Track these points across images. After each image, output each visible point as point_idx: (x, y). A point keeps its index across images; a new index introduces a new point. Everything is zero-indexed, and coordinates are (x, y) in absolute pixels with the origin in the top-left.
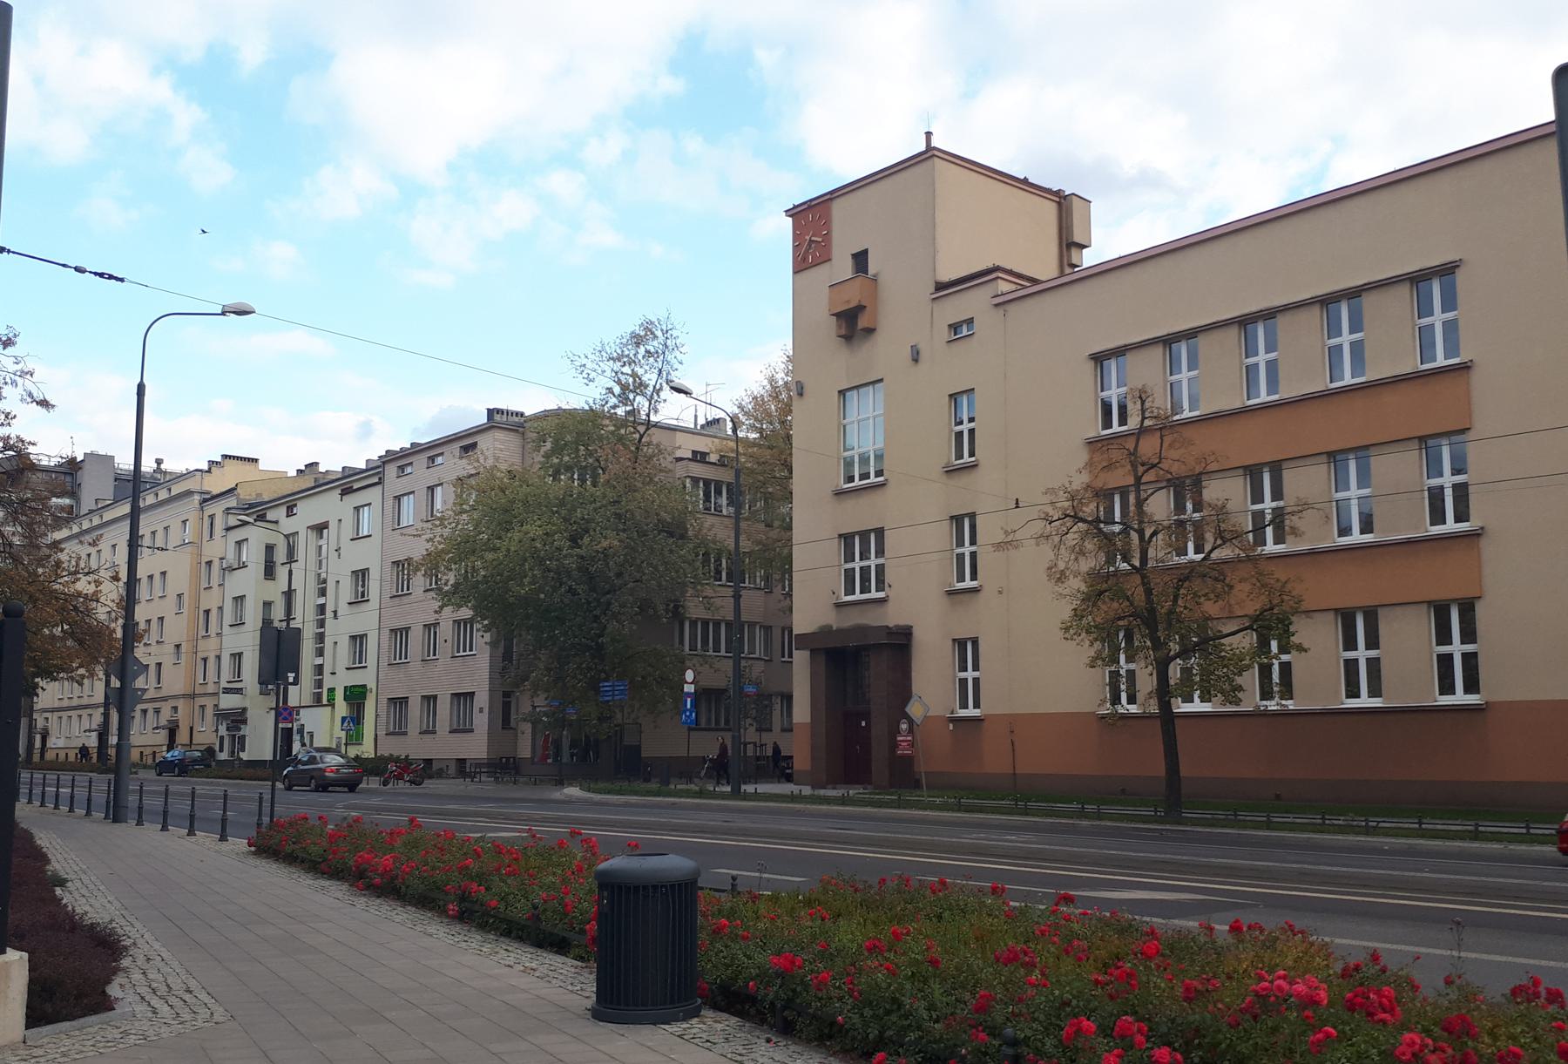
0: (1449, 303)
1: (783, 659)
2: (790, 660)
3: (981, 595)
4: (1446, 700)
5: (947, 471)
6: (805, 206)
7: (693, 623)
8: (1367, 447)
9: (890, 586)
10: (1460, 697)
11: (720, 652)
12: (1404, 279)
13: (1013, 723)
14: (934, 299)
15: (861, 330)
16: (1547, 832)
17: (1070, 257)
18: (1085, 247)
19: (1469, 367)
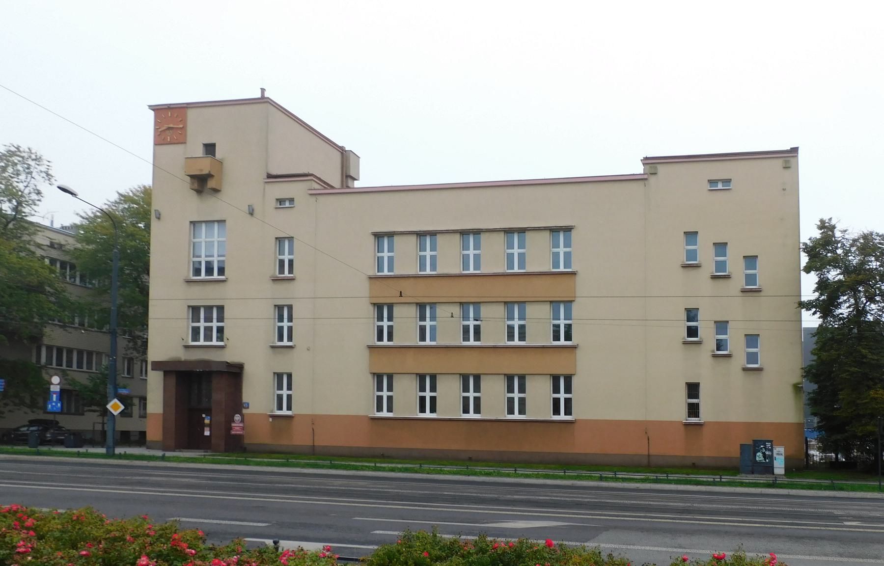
0: (567, 244)
1: (141, 378)
2: (146, 378)
3: (294, 350)
4: (556, 418)
5: (273, 280)
6: (166, 107)
7: (49, 348)
8: (525, 302)
9: (228, 339)
10: (562, 417)
11: (82, 368)
12: (548, 229)
13: (314, 420)
14: (266, 182)
15: (209, 189)
16: (642, 477)
17: (347, 182)
18: (356, 180)
19: (575, 274)
